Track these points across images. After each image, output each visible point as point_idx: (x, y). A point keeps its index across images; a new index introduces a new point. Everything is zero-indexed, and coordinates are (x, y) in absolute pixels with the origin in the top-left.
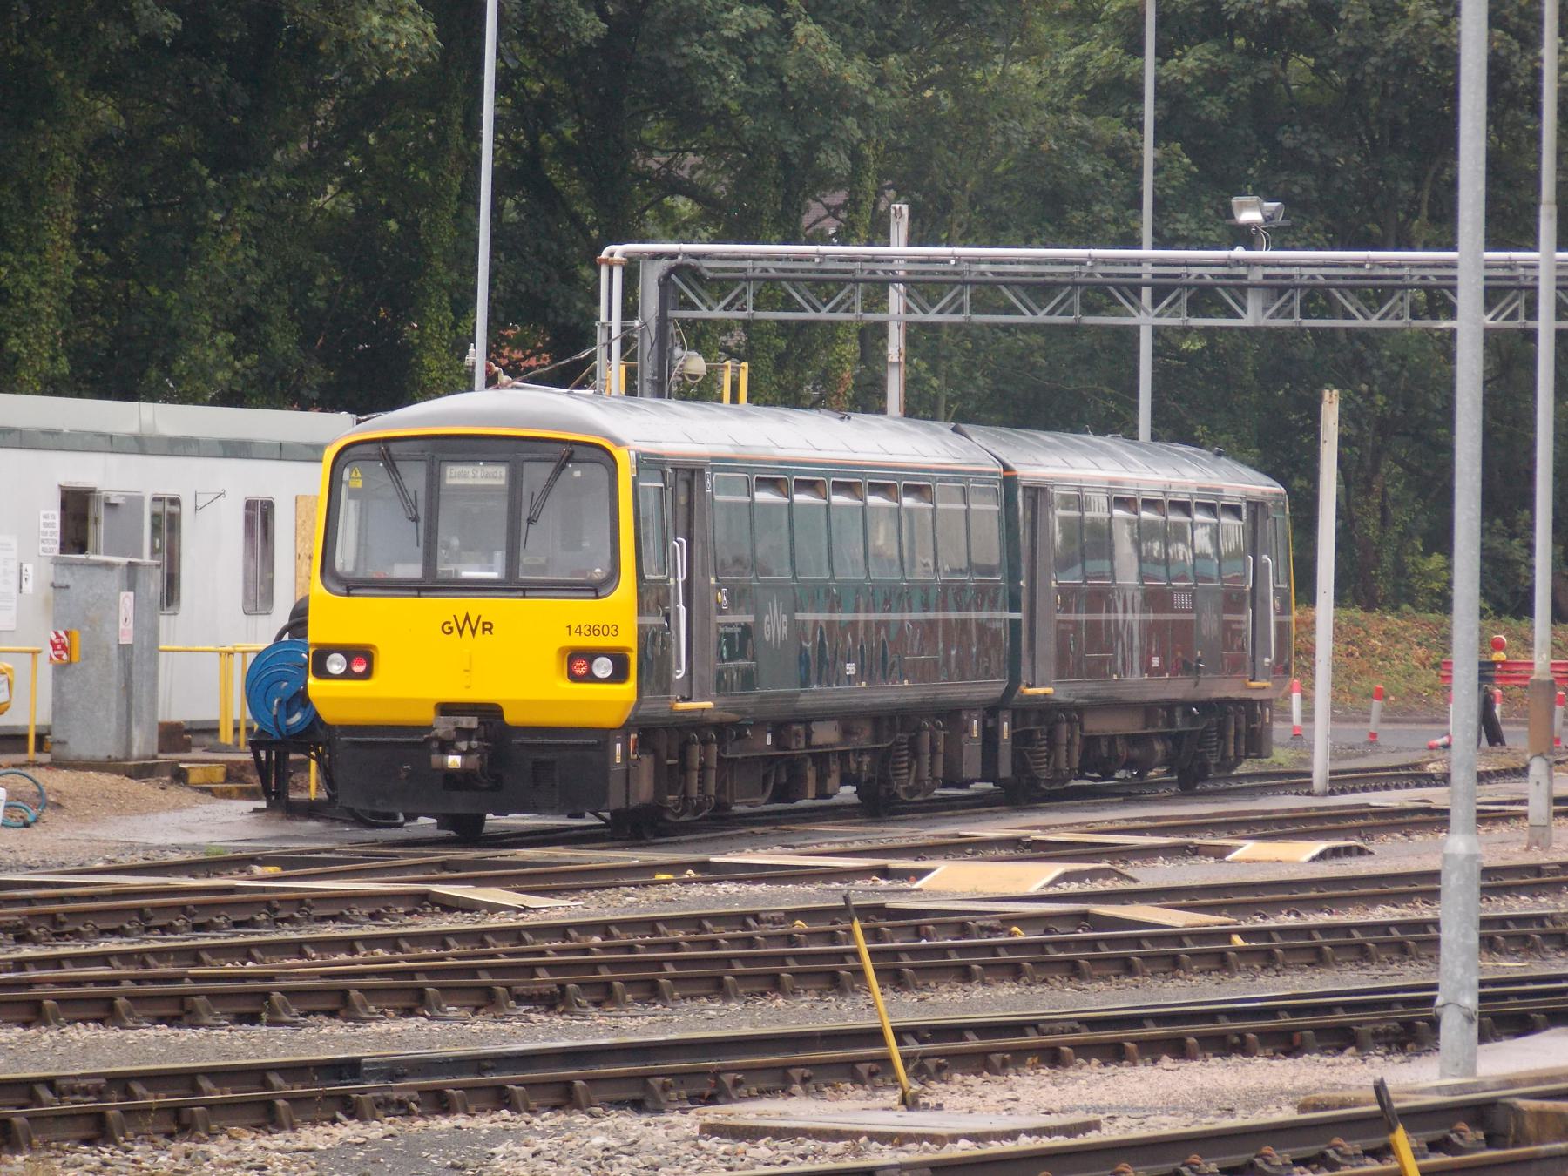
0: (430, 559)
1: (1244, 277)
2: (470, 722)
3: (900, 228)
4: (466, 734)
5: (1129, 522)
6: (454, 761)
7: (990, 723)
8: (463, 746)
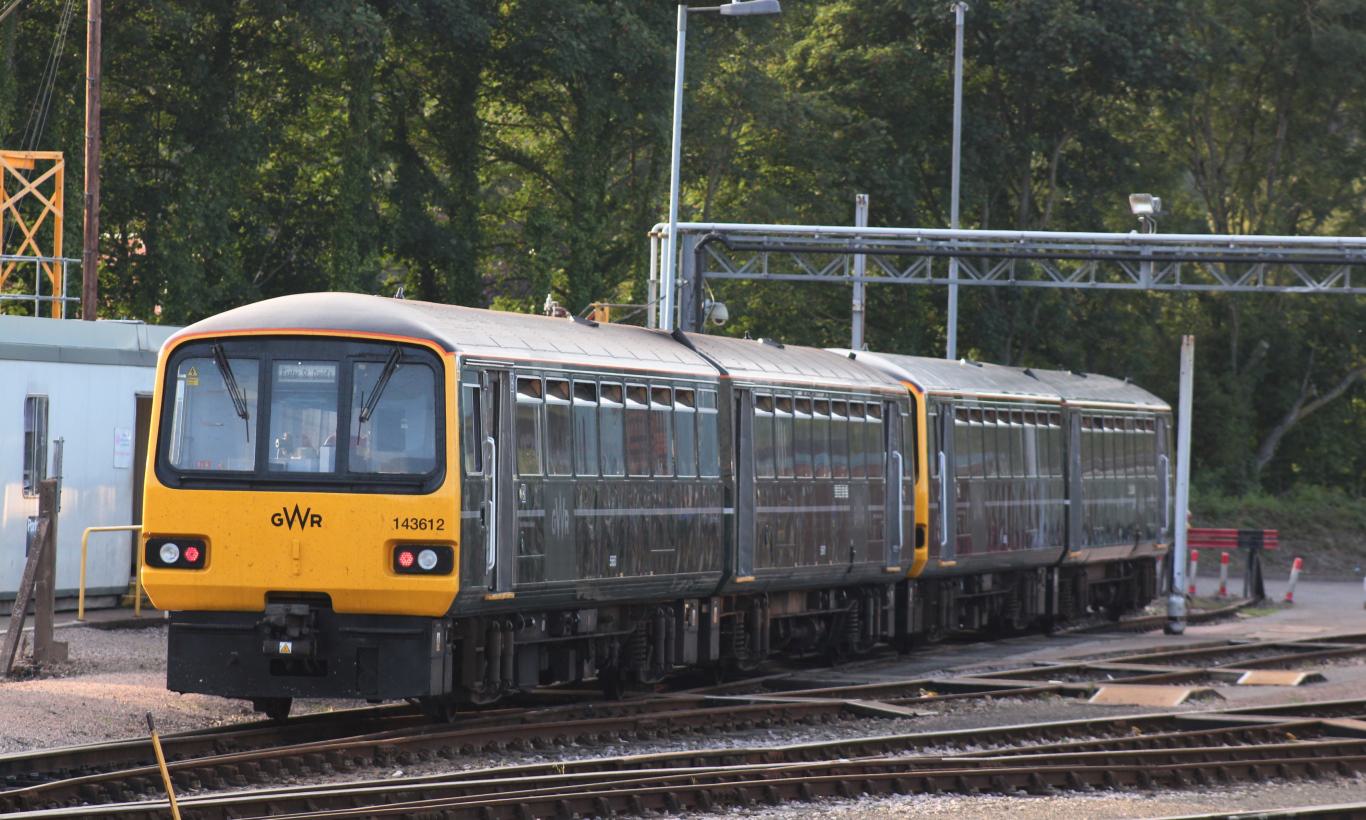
0: (343, 442)
1: (1138, 253)
2: (299, 609)
3: (862, 213)
4: (299, 619)
5: (614, 410)
6: (285, 647)
7: (704, 610)
8: (295, 632)
